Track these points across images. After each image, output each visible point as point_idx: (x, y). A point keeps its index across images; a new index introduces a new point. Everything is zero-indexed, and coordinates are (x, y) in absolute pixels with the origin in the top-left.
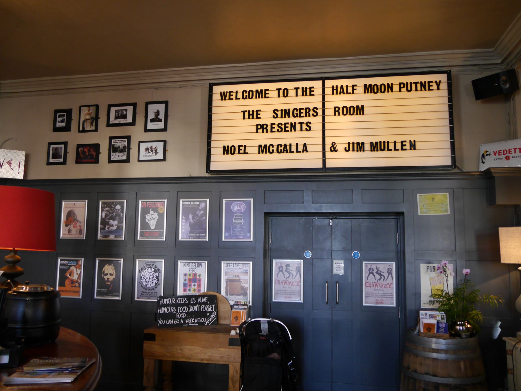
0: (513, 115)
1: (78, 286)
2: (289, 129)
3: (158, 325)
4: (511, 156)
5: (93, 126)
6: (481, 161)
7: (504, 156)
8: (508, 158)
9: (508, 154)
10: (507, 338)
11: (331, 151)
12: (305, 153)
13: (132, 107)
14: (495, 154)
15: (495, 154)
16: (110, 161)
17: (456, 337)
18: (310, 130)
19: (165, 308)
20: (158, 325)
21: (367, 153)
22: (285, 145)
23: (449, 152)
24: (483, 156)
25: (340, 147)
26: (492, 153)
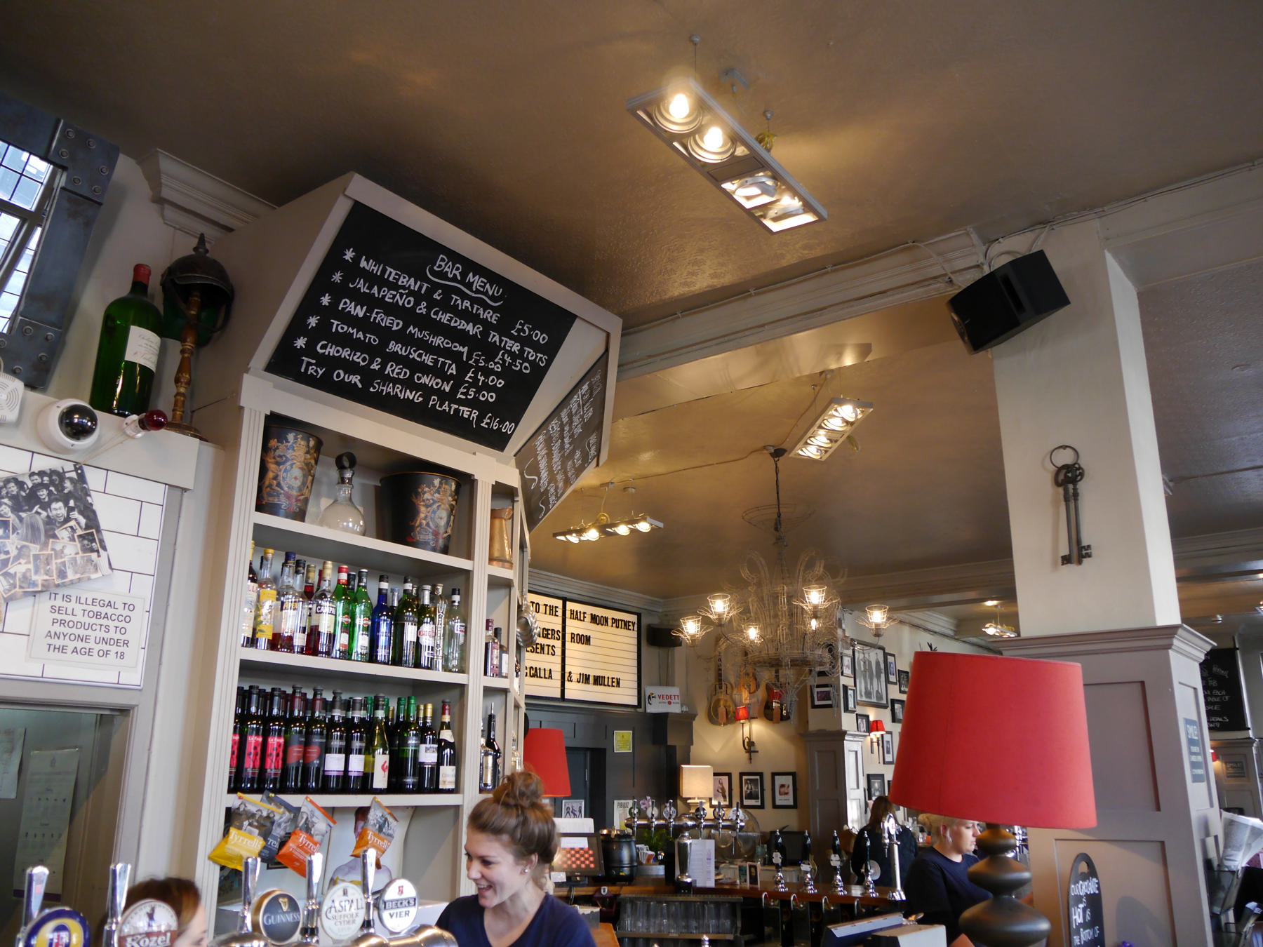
0: (442, 638)
1: (428, 476)
2: (539, 651)
3: (608, 529)
4: (672, 701)
5: (843, 685)
6: (647, 702)
7: (667, 701)
8: (670, 703)
9: (669, 700)
10: (953, 296)
11: (568, 680)
12: (550, 680)
13: (568, 603)
14: (660, 698)
15: (660, 698)
16: (761, 774)
17: (757, 175)
18: (554, 655)
19: (353, 382)
20: (608, 529)
21: (591, 687)
22: (536, 668)
23: (635, 692)
24: (649, 697)
25: (575, 677)
26: (657, 696)
